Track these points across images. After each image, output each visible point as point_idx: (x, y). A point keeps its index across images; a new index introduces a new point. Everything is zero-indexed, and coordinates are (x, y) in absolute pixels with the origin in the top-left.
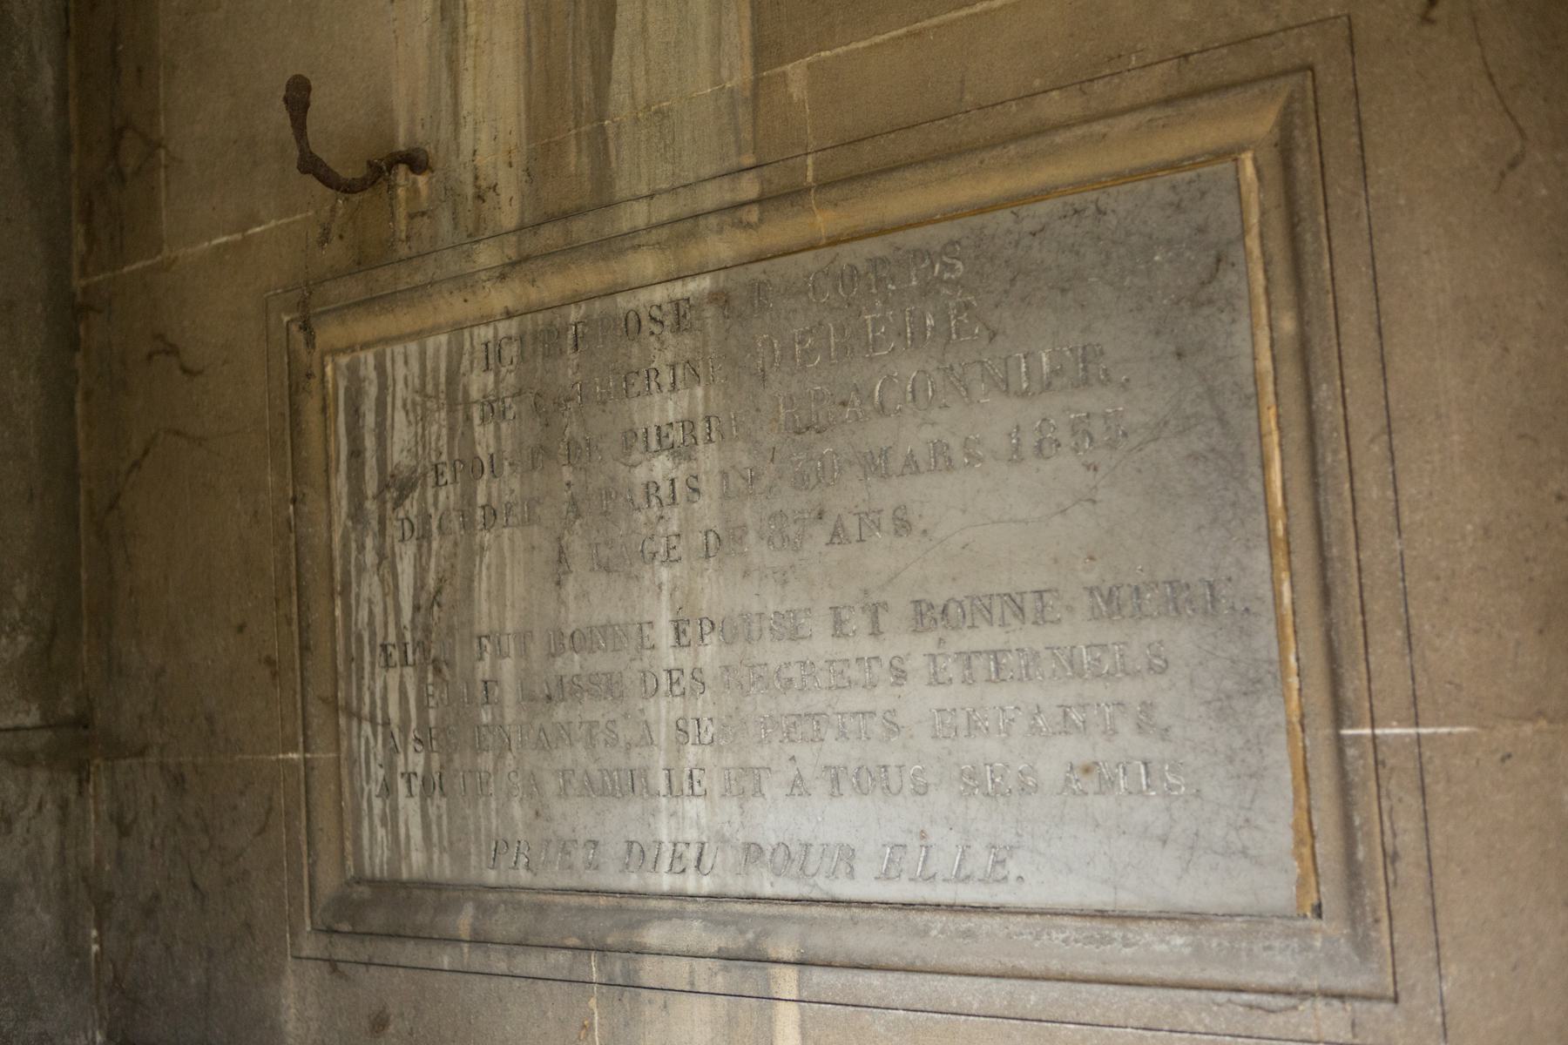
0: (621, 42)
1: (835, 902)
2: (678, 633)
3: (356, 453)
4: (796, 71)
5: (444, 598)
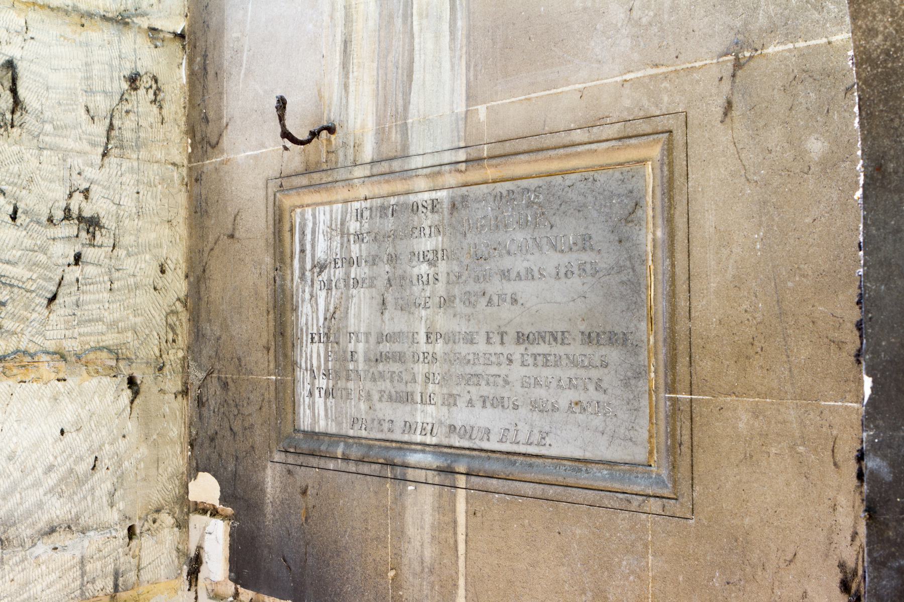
1: (482, 450)
2: (428, 337)
3: (303, 251)
5: (336, 316)
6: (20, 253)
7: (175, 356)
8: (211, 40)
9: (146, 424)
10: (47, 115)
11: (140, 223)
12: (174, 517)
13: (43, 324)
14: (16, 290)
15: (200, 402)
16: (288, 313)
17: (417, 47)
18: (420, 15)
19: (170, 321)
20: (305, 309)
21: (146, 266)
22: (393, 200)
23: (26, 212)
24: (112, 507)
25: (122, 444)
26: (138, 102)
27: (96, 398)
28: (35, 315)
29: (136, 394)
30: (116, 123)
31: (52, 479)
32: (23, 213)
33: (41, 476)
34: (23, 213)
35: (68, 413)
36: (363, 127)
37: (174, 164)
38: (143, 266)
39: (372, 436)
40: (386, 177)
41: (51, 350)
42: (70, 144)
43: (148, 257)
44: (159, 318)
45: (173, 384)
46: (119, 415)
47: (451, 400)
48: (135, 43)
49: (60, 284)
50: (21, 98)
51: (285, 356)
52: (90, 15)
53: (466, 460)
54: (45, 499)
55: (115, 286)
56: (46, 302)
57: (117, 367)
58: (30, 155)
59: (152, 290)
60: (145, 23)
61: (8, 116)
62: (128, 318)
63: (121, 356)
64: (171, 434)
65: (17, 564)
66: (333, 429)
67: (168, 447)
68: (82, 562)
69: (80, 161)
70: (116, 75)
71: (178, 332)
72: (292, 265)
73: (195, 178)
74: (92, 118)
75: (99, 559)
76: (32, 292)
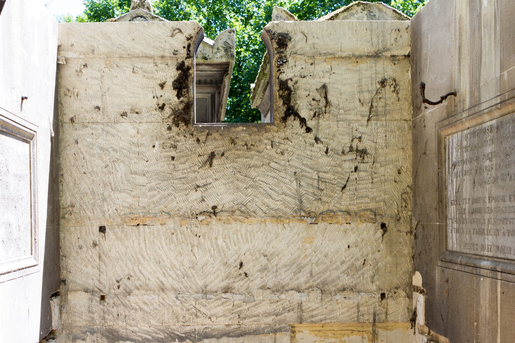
0: (483, 66)
1: (508, 259)
2: (489, 199)
3: (449, 158)
4: (505, 73)
5: (459, 191)
6: (329, 168)
7: (406, 214)
8: (418, 56)
9: (391, 246)
10: (341, 105)
11: (387, 151)
12: (406, 292)
13: (340, 198)
14: (328, 184)
15: (416, 237)
16: (444, 190)
17: (483, 44)
18: (484, 26)
19: (403, 197)
20: (450, 188)
21: (390, 171)
22: (477, 128)
23: (332, 150)
24: (373, 283)
25: (378, 255)
26: (386, 93)
27: (365, 232)
28: (336, 195)
29: (385, 231)
30: (374, 104)
31: (344, 267)
32: (331, 150)
33: (339, 265)
34: (331, 150)
35: (352, 238)
36: (466, 91)
37: (405, 120)
38: (389, 171)
39: (471, 253)
40: (473, 116)
41: (343, 210)
42: (352, 117)
43: (391, 166)
44: (397, 195)
45: (405, 228)
46: (376, 241)
47: (497, 233)
48: (384, 65)
49: (347, 181)
50: (329, 100)
51: (443, 212)
52: (361, 57)
53: (502, 264)
54: (341, 275)
55: (374, 181)
56: (341, 189)
57: (375, 219)
58: (333, 124)
59: (394, 182)
60: (388, 54)
61: (324, 109)
62: (381, 196)
63: (377, 213)
64: (404, 252)
65: (328, 302)
66: (458, 250)
67: (403, 258)
68: (358, 306)
69: (357, 124)
70: (374, 82)
71: (408, 202)
72: (445, 166)
73: (414, 126)
74: (362, 104)
75: (366, 306)
76: (335, 184)
